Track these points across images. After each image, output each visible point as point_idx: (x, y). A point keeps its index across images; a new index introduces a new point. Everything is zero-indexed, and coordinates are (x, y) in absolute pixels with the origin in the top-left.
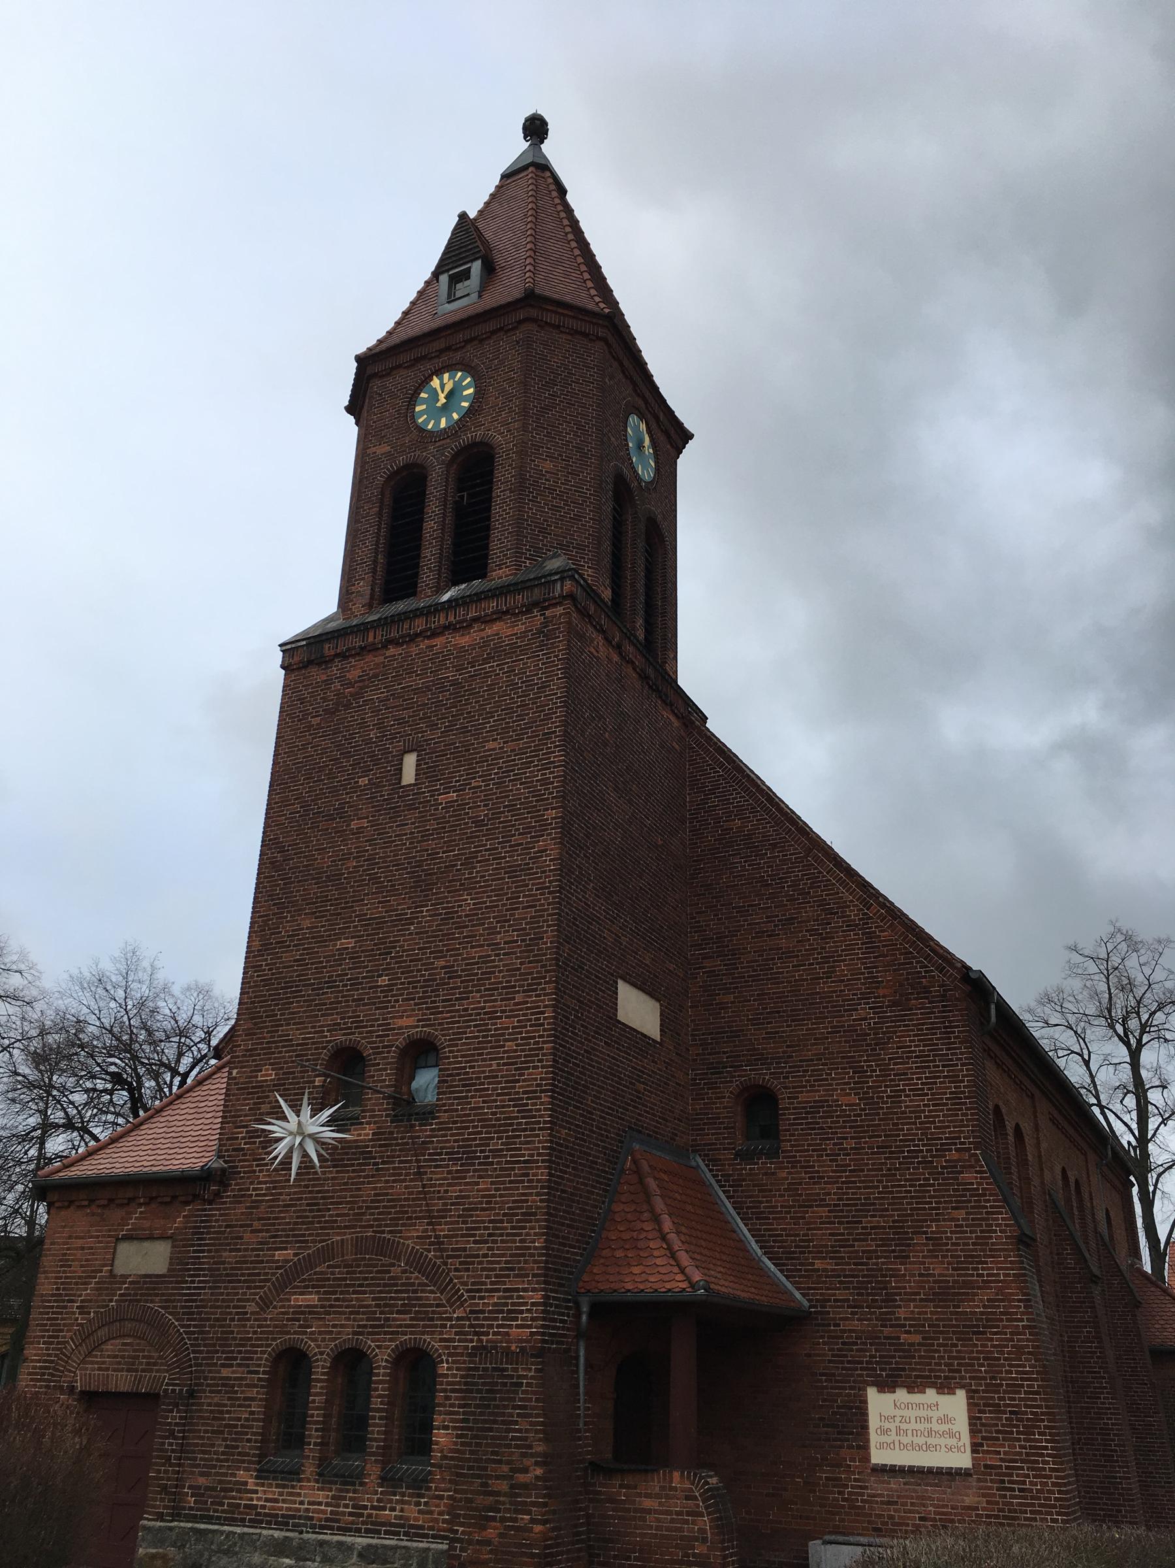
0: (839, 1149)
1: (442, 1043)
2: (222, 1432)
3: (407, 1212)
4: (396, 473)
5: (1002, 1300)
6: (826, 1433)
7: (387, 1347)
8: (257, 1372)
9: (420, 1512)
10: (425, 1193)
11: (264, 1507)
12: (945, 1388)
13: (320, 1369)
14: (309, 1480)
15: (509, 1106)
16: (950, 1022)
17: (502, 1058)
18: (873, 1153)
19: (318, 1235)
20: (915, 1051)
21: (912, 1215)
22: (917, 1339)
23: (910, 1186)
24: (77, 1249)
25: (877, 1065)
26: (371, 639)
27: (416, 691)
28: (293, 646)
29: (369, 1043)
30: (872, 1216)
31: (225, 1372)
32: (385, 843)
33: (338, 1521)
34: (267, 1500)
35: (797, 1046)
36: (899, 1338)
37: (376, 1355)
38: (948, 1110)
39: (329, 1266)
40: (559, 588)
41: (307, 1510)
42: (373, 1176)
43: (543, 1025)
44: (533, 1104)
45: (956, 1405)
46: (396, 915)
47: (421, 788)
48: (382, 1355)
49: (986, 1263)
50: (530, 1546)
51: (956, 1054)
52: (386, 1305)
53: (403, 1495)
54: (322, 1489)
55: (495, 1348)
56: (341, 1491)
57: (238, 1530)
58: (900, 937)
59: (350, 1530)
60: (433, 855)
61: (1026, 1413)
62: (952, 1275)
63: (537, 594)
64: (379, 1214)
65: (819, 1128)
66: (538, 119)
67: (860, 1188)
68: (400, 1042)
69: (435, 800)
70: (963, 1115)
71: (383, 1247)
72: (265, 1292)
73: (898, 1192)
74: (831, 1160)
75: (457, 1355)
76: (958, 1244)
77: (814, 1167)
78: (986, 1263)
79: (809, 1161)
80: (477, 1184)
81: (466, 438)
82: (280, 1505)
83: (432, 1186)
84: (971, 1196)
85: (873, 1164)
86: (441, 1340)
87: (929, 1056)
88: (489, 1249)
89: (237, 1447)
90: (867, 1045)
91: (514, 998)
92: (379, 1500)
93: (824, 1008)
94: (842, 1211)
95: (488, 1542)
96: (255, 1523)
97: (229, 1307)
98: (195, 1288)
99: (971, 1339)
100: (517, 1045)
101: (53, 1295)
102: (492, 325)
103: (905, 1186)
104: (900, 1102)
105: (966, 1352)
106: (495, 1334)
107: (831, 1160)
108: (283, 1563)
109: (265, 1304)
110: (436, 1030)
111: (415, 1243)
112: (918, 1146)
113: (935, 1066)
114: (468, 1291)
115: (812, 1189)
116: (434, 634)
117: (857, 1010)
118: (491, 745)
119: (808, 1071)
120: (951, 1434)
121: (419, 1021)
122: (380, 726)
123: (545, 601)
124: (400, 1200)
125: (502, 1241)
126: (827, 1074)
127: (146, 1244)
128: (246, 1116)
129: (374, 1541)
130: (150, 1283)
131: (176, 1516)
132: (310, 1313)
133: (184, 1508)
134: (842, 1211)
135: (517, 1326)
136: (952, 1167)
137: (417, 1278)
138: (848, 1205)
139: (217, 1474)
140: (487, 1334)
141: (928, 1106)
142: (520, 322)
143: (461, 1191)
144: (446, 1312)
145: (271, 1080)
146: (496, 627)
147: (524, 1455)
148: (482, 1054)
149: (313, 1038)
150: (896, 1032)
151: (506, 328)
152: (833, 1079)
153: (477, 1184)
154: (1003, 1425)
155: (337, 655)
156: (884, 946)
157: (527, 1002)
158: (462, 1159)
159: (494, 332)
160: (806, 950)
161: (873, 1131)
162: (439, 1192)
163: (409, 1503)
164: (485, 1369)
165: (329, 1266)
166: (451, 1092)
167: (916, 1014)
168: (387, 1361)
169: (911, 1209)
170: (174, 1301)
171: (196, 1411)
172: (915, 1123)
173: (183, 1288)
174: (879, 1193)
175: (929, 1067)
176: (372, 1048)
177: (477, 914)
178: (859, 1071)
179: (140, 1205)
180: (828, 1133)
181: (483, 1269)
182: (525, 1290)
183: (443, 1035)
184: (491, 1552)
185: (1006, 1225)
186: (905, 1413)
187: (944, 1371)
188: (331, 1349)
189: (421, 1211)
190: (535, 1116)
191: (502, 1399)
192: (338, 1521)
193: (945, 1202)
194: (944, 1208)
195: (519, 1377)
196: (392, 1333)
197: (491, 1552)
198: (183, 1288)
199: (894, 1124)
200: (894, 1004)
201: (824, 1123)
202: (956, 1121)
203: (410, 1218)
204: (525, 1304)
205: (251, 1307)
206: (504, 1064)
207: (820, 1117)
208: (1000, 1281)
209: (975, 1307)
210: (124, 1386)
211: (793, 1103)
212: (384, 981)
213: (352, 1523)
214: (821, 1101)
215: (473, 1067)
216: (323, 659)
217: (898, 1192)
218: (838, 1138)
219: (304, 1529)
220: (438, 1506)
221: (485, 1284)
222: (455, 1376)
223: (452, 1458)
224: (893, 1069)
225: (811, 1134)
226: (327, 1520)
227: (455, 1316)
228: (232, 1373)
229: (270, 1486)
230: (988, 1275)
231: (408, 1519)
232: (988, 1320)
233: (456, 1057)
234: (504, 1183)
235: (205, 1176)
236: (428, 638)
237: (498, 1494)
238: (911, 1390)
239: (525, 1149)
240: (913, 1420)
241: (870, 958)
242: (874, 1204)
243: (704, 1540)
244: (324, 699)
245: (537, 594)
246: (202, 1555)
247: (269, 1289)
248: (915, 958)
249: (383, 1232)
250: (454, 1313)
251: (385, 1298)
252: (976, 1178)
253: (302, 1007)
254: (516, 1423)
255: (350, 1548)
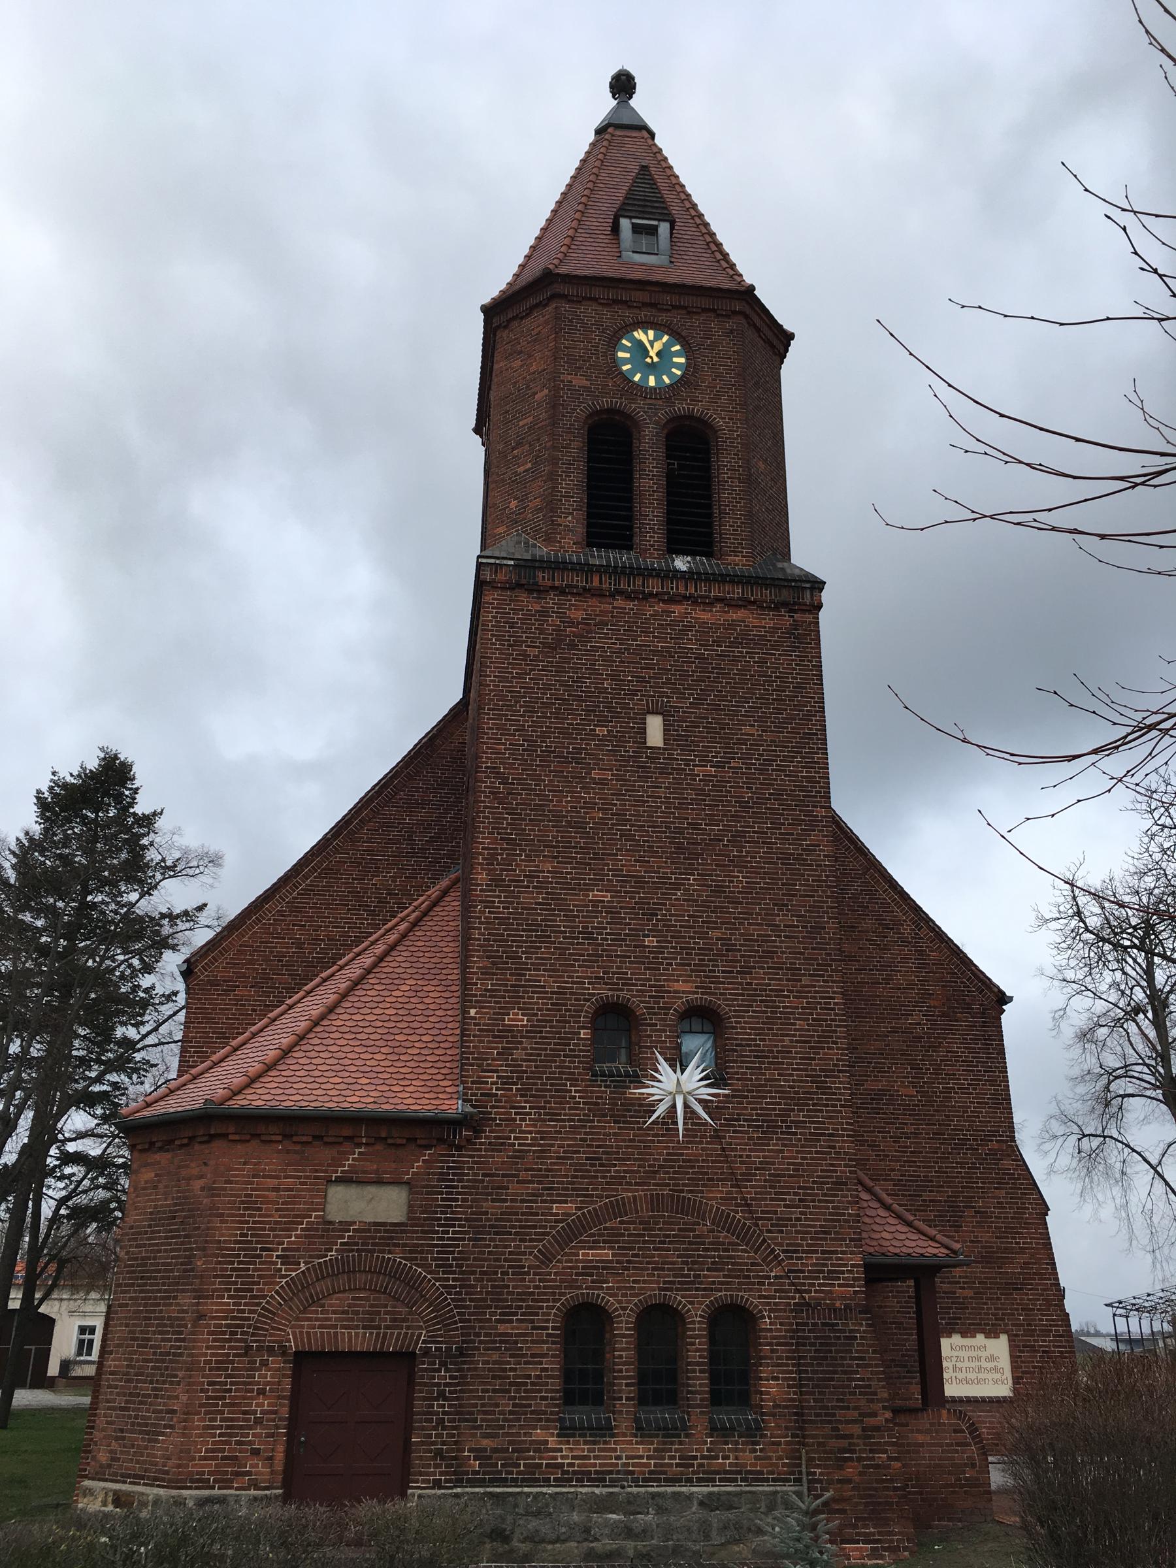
0: (901, 1133)
1: (727, 1013)
2: (509, 1391)
3: (707, 1173)
4: (597, 413)
5: (1035, 1264)
6: (898, 1372)
7: (701, 1303)
8: (546, 1328)
9: (756, 1458)
10: (726, 1156)
11: (572, 1465)
12: (992, 1333)
13: (624, 1327)
14: (625, 1435)
15: (807, 1082)
16: (989, 1035)
17: (794, 1036)
18: (928, 1138)
19: (603, 1190)
20: (961, 1057)
21: (963, 1192)
22: (969, 1293)
23: (961, 1168)
24: (268, 1190)
25: (930, 1065)
26: (596, 583)
27: (655, 652)
28: (498, 562)
29: (641, 1002)
30: (930, 1191)
31: (501, 1329)
32: (635, 801)
33: (665, 1473)
34: (574, 1458)
35: (860, 1040)
36: (955, 1293)
37: (689, 1310)
38: (989, 1108)
39: (621, 1222)
40: (808, 596)
41: (627, 1465)
42: (663, 1136)
43: (833, 1009)
44: (832, 1083)
45: (1000, 1347)
46: (657, 878)
47: (673, 754)
48: (696, 1312)
49: (1021, 1233)
50: (891, 1481)
51: (994, 1062)
52: (694, 1263)
53: (737, 1443)
54: (641, 1443)
55: (820, 1305)
56: (665, 1443)
57: (550, 1490)
58: (946, 958)
59: (680, 1480)
60: (694, 825)
61: (1054, 1352)
62: (996, 1243)
63: (785, 595)
64: (674, 1173)
65: (883, 1114)
66: (623, 75)
67: (919, 1167)
68: (678, 1005)
69: (690, 770)
70: (1001, 1113)
71: (682, 1206)
72: (544, 1246)
73: (950, 1172)
74: (894, 1142)
75: (779, 1310)
76: (1000, 1218)
77: (879, 1146)
78: (1021, 1233)
79: (875, 1141)
80: (782, 1151)
81: (682, 407)
82: (592, 1461)
83: (732, 1150)
84: (1009, 1179)
85: (930, 1148)
86: (760, 1297)
87: (972, 1062)
88: (801, 1213)
89: (530, 1406)
90: (922, 1046)
91: (801, 980)
92: (709, 1450)
93: (884, 1009)
94: (905, 1185)
95: (849, 1481)
96: (560, 1482)
97: (499, 1260)
98: (449, 1239)
99: (1012, 1294)
100: (808, 1025)
101: (237, 1242)
102: (706, 303)
103: (957, 1167)
104: (951, 1097)
105: (1008, 1304)
106: (816, 1292)
107: (894, 1142)
108: (610, 1519)
109: (547, 1258)
110: (719, 999)
111: (719, 1204)
112: (966, 1135)
113: (978, 1071)
114: (784, 1251)
115: (878, 1165)
116: (672, 600)
117: (912, 1015)
118: (746, 730)
119: (871, 1063)
120: (996, 1370)
121: (697, 987)
122: (615, 676)
123: (795, 604)
124: (698, 1161)
125: (814, 1207)
126: (888, 1067)
127: (372, 1190)
128: (493, 1059)
129: (712, 1489)
130: (385, 1233)
131: (459, 1482)
132: (604, 1268)
133: (467, 1473)
134: (905, 1185)
135: (840, 1285)
136: (993, 1155)
137: (726, 1237)
138: (910, 1181)
139: (508, 1435)
140: (810, 1292)
141: (973, 1103)
142: (734, 313)
143: (764, 1157)
144: (762, 1271)
145: (522, 1026)
146: (741, 614)
147: (872, 1401)
148: (772, 1029)
149: (572, 988)
150: (945, 1038)
151: (718, 312)
152: (894, 1072)
153: (782, 1151)
154: (1037, 1362)
155: (553, 588)
156: (933, 964)
157: (814, 986)
158: (762, 1126)
159: (705, 310)
160: (866, 957)
161: (929, 1120)
162: (741, 1156)
163: (744, 1451)
164: (814, 1324)
165: (621, 1222)
166: (742, 1062)
167: (961, 1026)
168: (701, 1316)
169: (962, 1187)
170: (422, 1252)
171: (469, 1369)
172: (963, 1116)
173: (433, 1238)
174: (936, 1172)
175: (973, 1071)
176: (646, 1008)
177: (752, 893)
178: (916, 1067)
179: (359, 1145)
180: (890, 1118)
181: (797, 1232)
182: (843, 1252)
183: (727, 1005)
184: (853, 1489)
185: (1036, 1204)
186: (961, 1354)
187: (991, 1320)
188: (635, 1305)
189: (722, 1174)
190: (835, 1094)
191: (837, 1352)
192: (665, 1473)
193: (989, 1183)
194: (989, 1188)
195: (851, 1331)
196: (705, 1289)
197: (853, 1489)
198: (433, 1238)
199: (946, 1116)
200: (943, 1015)
201: (887, 1109)
202: (995, 1118)
203: (712, 1179)
204: (845, 1265)
205: (527, 1261)
206: (797, 1041)
207: (883, 1104)
208: (1033, 1248)
209: (1014, 1268)
210: (362, 1343)
211: (859, 1089)
212: (651, 942)
213: (682, 1473)
214: (883, 1090)
215: (764, 1040)
216: (535, 587)
217: (950, 1172)
218: (900, 1123)
219: (626, 1484)
220: (776, 1451)
221: (801, 1245)
222: (780, 1330)
223: (786, 1407)
224: (944, 1070)
225: (876, 1118)
226: (651, 1472)
227: (773, 1274)
228: (512, 1329)
229: (578, 1443)
230: (1024, 1243)
231: (745, 1465)
232: (1024, 1279)
233: (744, 1028)
234: (810, 1153)
235: (458, 1123)
236: (664, 601)
237: (851, 1436)
238: (988, 1335)
239: (829, 1123)
240: (966, 1359)
241: (921, 972)
242: (932, 1181)
243: (973, 1466)
244: (542, 631)
245: (785, 595)
246: (503, 1520)
247: (549, 1241)
248: (959, 978)
249: (682, 1191)
250: (772, 1271)
251: (692, 1256)
252: (1013, 1165)
253: (553, 954)
254: (857, 1372)
255: (690, 1497)
